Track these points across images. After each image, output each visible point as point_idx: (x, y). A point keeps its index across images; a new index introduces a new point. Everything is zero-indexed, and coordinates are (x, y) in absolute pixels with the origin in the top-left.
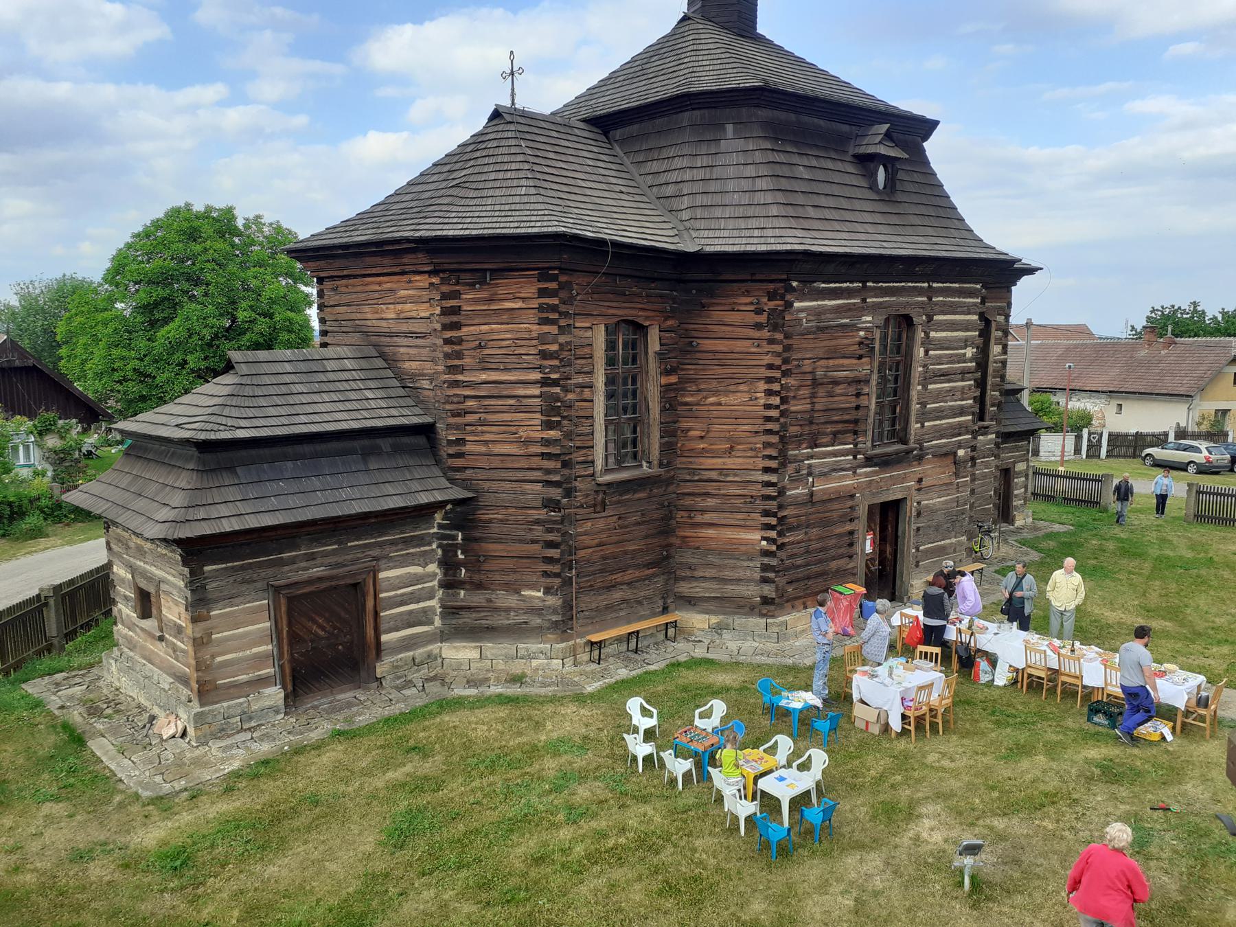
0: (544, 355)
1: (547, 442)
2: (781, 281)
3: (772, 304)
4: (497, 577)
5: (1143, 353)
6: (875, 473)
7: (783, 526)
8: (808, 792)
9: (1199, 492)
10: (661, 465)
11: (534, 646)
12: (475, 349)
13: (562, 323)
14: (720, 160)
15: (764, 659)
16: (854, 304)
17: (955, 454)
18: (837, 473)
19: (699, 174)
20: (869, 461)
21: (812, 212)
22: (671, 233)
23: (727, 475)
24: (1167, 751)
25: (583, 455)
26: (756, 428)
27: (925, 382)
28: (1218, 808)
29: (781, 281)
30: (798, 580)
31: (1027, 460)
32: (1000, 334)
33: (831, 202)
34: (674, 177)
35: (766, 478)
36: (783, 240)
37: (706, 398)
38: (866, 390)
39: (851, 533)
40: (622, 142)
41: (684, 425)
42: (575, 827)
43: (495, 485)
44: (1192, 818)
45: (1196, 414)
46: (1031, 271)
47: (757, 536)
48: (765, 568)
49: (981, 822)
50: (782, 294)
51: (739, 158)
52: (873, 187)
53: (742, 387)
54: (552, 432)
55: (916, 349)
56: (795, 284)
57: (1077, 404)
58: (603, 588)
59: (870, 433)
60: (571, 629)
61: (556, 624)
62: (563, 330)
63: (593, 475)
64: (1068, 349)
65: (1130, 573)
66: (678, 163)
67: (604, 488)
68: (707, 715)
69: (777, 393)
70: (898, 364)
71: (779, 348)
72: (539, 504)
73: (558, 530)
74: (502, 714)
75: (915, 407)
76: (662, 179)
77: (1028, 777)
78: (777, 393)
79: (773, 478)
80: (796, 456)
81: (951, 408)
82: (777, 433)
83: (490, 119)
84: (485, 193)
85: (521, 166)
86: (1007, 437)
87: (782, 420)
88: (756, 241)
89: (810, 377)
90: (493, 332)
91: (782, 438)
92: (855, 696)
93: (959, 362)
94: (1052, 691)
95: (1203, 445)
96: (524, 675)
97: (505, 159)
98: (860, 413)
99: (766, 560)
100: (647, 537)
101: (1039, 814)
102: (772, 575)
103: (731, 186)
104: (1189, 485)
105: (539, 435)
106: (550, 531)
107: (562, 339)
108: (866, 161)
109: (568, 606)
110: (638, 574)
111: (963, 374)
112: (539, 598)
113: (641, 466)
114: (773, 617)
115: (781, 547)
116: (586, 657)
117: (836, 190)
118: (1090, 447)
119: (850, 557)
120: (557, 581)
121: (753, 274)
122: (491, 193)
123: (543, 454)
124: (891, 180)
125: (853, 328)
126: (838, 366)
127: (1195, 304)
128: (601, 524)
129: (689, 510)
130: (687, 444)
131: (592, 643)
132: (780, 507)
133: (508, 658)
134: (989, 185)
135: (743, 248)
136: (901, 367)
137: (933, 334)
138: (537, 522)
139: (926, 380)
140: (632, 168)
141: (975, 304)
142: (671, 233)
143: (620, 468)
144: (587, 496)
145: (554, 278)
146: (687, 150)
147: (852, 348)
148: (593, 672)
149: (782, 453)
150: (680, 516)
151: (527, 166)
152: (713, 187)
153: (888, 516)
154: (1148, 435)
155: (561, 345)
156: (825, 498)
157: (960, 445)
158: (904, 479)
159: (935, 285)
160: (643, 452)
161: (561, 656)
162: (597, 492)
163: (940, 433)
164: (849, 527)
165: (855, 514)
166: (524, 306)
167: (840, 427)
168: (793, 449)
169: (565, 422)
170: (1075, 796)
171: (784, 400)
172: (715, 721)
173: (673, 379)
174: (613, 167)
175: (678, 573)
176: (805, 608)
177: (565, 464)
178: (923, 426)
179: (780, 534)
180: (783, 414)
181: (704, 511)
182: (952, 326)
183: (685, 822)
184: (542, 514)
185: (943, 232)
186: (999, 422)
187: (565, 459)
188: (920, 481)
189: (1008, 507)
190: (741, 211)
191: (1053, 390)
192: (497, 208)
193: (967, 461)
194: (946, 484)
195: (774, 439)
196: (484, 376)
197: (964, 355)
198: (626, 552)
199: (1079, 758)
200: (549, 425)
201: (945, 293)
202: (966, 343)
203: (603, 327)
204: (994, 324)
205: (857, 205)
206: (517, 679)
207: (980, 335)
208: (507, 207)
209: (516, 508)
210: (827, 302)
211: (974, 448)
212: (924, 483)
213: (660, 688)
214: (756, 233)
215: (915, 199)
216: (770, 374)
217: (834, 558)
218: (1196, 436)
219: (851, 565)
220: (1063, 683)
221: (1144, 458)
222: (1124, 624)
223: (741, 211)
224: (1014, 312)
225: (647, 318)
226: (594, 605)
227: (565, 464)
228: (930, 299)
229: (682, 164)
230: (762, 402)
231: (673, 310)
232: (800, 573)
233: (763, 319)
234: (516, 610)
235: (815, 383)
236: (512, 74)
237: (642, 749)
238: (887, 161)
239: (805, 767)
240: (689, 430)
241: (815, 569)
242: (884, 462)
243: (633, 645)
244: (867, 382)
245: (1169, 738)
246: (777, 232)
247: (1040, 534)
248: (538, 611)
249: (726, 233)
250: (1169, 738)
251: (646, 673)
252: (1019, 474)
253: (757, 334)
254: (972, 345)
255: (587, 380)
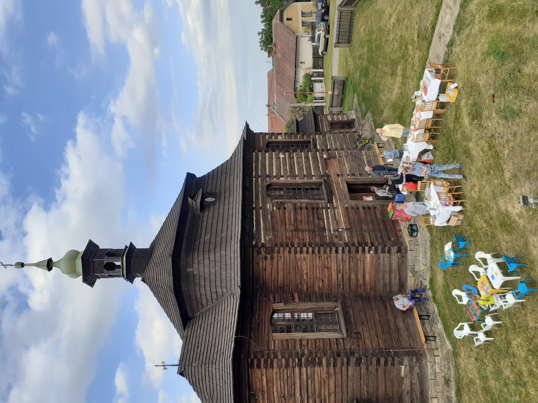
0: (287, 366)
1: (328, 365)
2: (253, 249)
3: (263, 253)
4: (395, 389)
5: (279, 55)
6: (335, 197)
7: (362, 244)
8: (498, 264)
9: (338, 43)
10: (336, 301)
11: (429, 371)
12: (285, 399)
13: (272, 357)
14: (202, 274)
15: (428, 255)
16: (262, 213)
17: (325, 159)
18: (336, 217)
19: (208, 284)
20: (330, 201)
21: (224, 234)
22: (232, 299)
23: (340, 269)
24: (463, 87)
25: (334, 344)
26: (317, 257)
27: (294, 176)
28: (491, 72)
29: (253, 249)
30: (388, 235)
31: (327, 115)
32: (273, 137)
33: (220, 224)
34: (208, 294)
35: (340, 252)
36: (236, 250)
37: (304, 280)
38: (299, 204)
39: (364, 208)
40: (193, 312)
41: (317, 289)
42: (527, 384)
43: (350, 391)
44: (497, 85)
45: (304, 34)
46: (247, 126)
47: (368, 256)
48: (383, 251)
49: (508, 183)
50: (258, 248)
51: (202, 267)
52: (214, 203)
53: (299, 264)
54: (324, 362)
55: (281, 182)
56: (254, 243)
57: (301, 80)
58: (398, 333)
59: (318, 201)
60: (420, 351)
61: (418, 360)
62: (276, 357)
63: (343, 339)
64: (278, 84)
65: (375, 76)
66: (203, 292)
67: (349, 333)
68: (460, 298)
69: (301, 249)
70: (287, 189)
71: (282, 249)
72: (358, 368)
73: (371, 358)
74: (467, 398)
75: (306, 180)
76: (209, 298)
77: (481, 154)
78: (301, 249)
79: (340, 249)
80: (329, 238)
81: (306, 163)
82: (319, 248)
83: (183, 376)
84: (215, 388)
85: (203, 368)
86: (317, 130)
87: (313, 246)
88: (236, 262)
89: (294, 233)
90: (277, 391)
91: (322, 245)
92: (445, 224)
93: (286, 161)
94: (435, 130)
95: (317, 33)
96: (444, 377)
97: (200, 375)
98: (309, 207)
99: (379, 251)
100: (371, 309)
101: (501, 155)
102: (387, 248)
103: (213, 270)
104: (335, 47)
105: (325, 368)
106: (371, 363)
107: (280, 357)
108: (203, 206)
109: (408, 354)
110: (390, 314)
111: (291, 158)
112: (405, 368)
113: (337, 311)
114: (407, 247)
115: (373, 245)
116: (433, 343)
117: (215, 222)
118: (319, 76)
119: (375, 208)
120: (396, 359)
121: (250, 262)
122: (215, 385)
123: (334, 366)
124: (212, 195)
125: (272, 213)
126: (289, 219)
127: (259, 34)
128: (367, 334)
129: (357, 286)
130: (326, 288)
131: (426, 340)
132: (354, 245)
133: (436, 384)
134: (214, 150)
135: (239, 269)
136: (288, 187)
137: (274, 174)
138: (367, 369)
139: (294, 176)
140: (205, 309)
141: (262, 155)
142: (232, 299)
143: (339, 323)
144: (353, 343)
145: (252, 361)
146: (197, 288)
147: (281, 213)
148: (441, 341)
149: (328, 245)
150: (360, 290)
151: (203, 366)
152: (213, 278)
153: (356, 189)
154: (314, 50)
155: (282, 358)
156: (348, 222)
157: (322, 157)
158: (338, 183)
159: (254, 175)
160: (330, 310)
161: (433, 357)
162: (351, 337)
163: (317, 167)
164: (361, 209)
165: (355, 206)
166: (265, 375)
167: (315, 216)
168: (326, 240)
169: (318, 354)
170: (490, 135)
171: (305, 245)
172: (463, 294)
173: (296, 295)
174: (204, 319)
175: (388, 291)
176: (401, 230)
177: (339, 355)
178: (314, 176)
179: (367, 245)
180: (310, 246)
181: (357, 280)
182: (271, 165)
183: (520, 327)
184: (363, 367)
185: (232, 171)
186: (311, 134)
187: (337, 354)
188: (338, 175)
189: (348, 122)
190: (223, 267)
191: (295, 89)
192: (221, 385)
193: (329, 153)
194: (339, 162)
195: (322, 249)
196: (298, 395)
197: (283, 158)
198: (380, 320)
199: (468, 127)
200: (320, 364)
201: (257, 171)
202: (278, 158)
203: (274, 334)
204: (270, 140)
205: (221, 211)
206: (447, 382)
207: (274, 151)
208: (221, 380)
209: (361, 380)
210: (262, 226)
211: (323, 150)
212: (339, 173)
213: (447, 311)
214: (233, 261)
215: (219, 183)
216: (293, 251)
217: (376, 217)
218: (314, 33)
219: (379, 208)
220: (432, 125)
221: (323, 55)
222: (400, 86)
223: (223, 267)
224: (264, 131)
225: (269, 310)
226: (407, 338)
227: (339, 355)
228: (260, 176)
229: (203, 291)
230: (305, 255)
231: (266, 297)
232: (384, 234)
233: (269, 256)
234: (411, 379)
235: (296, 230)
236: (164, 366)
237: (482, 337)
238: (203, 197)
239: (485, 261)
240: (319, 287)
241: (382, 226)
242: (331, 194)
243: (426, 317)
244: (295, 204)
245: (456, 85)
246: (232, 252)
247: (359, 109)
248: (411, 368)
249: (233, 274)
250: (456, 85)
251: (439, 315)
252: (333, 118)
253: (276, 258)
254: (278, 155)
255: (298, 342)
